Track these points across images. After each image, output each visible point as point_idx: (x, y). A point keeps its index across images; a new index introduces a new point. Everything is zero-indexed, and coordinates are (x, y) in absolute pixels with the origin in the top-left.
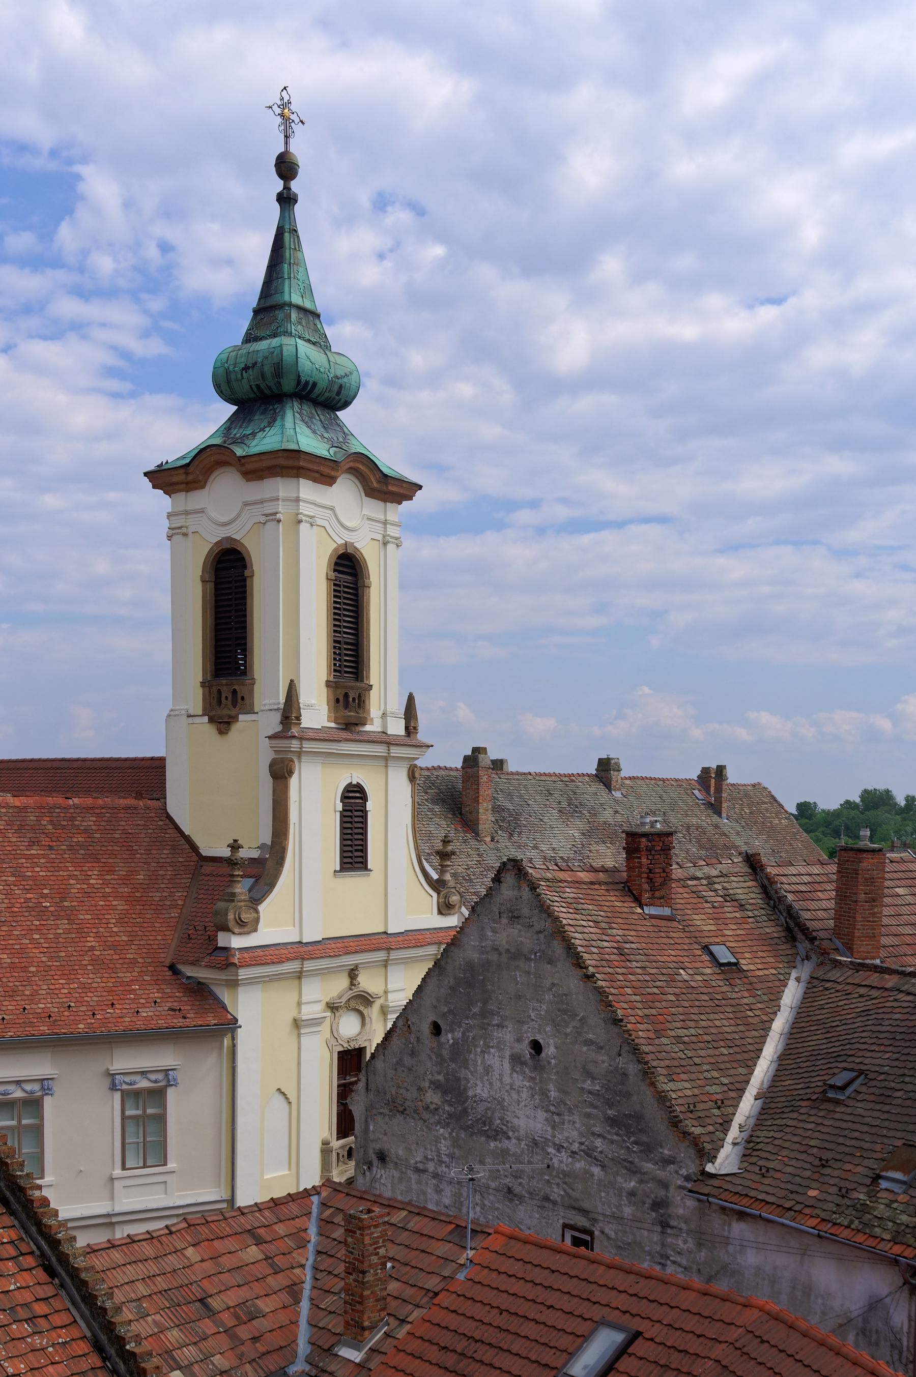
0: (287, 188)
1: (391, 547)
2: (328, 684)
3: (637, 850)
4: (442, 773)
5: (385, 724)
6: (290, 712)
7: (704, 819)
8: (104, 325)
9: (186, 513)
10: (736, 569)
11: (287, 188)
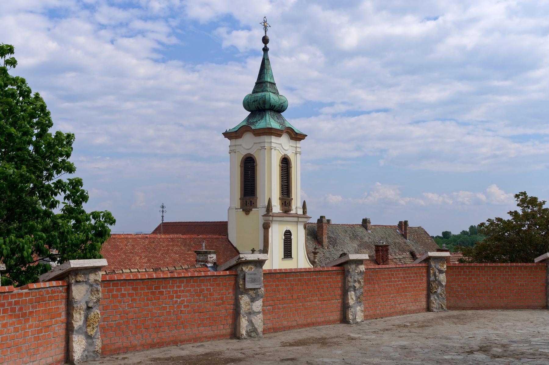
0: (266, 46)
1: (298, 155)
2: (280, 199)
3: (379, 250)
4: (310, 225)
5: (297, 211)
6: (269, 208)
7: (400, 240)
8: (153, 32)
9: (235, 146)
10: (417, 131)
11: (266, 46)
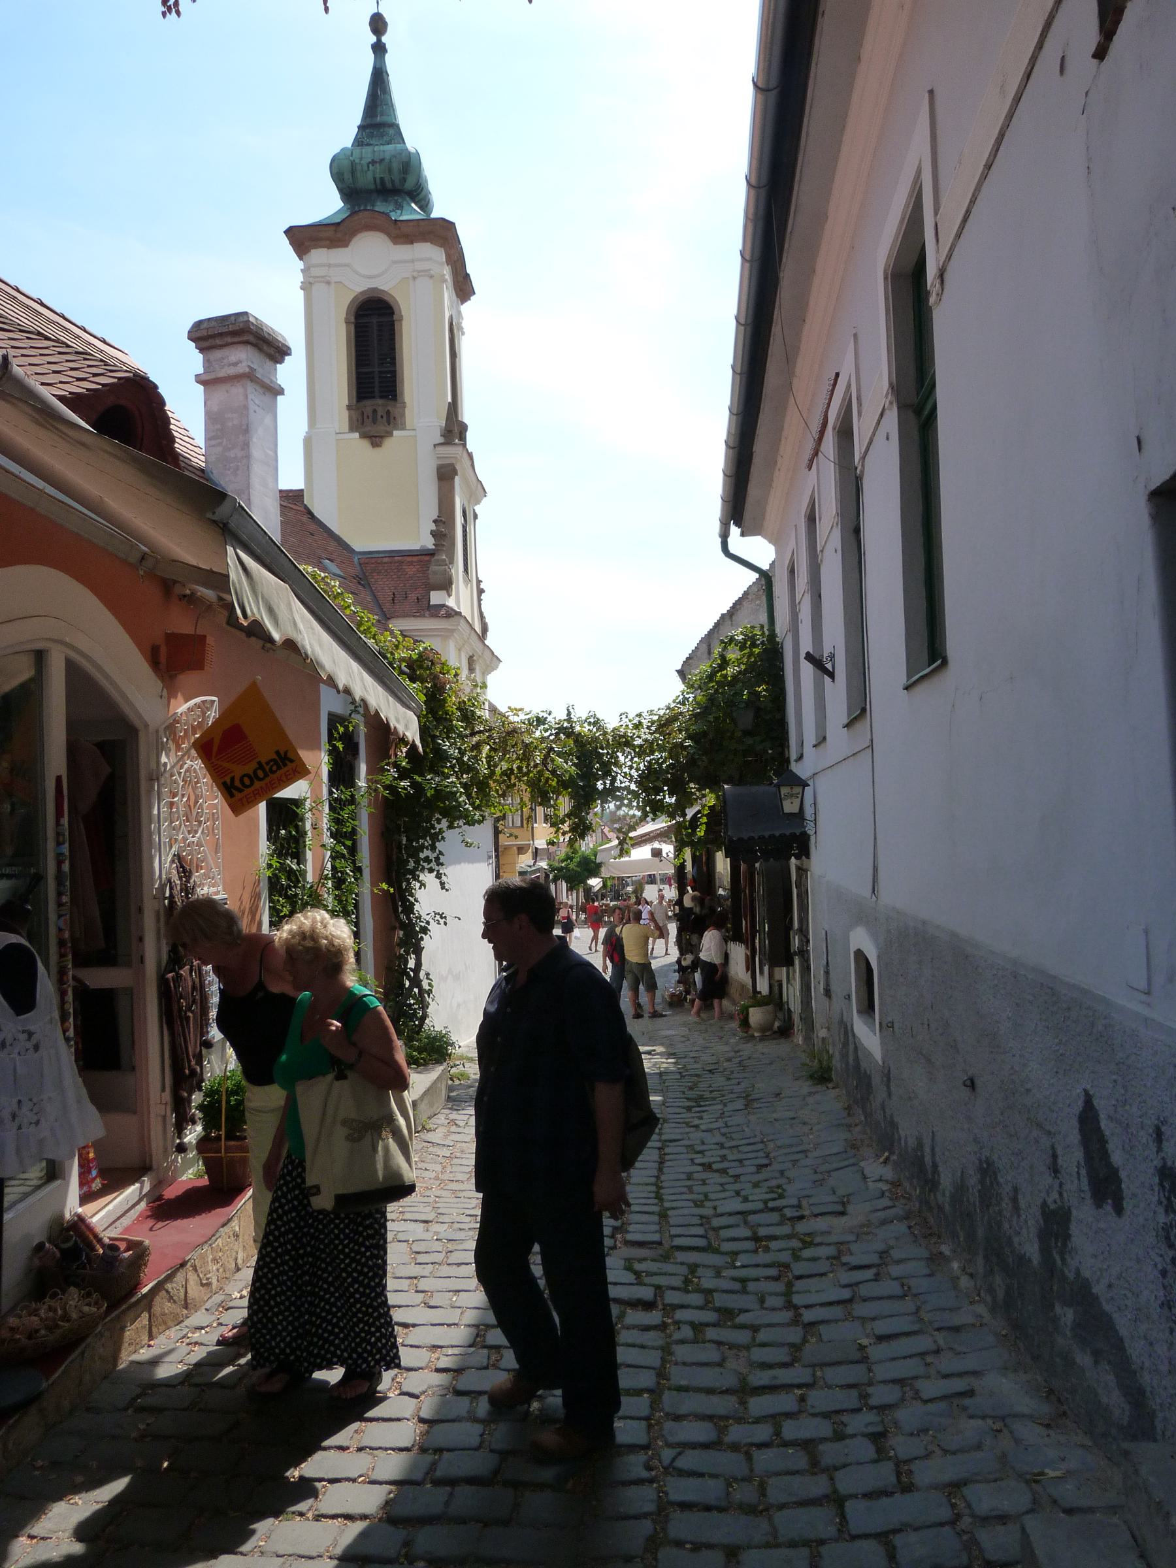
0: (379, 40)
9: (329, 266)
11: (379, 40)
